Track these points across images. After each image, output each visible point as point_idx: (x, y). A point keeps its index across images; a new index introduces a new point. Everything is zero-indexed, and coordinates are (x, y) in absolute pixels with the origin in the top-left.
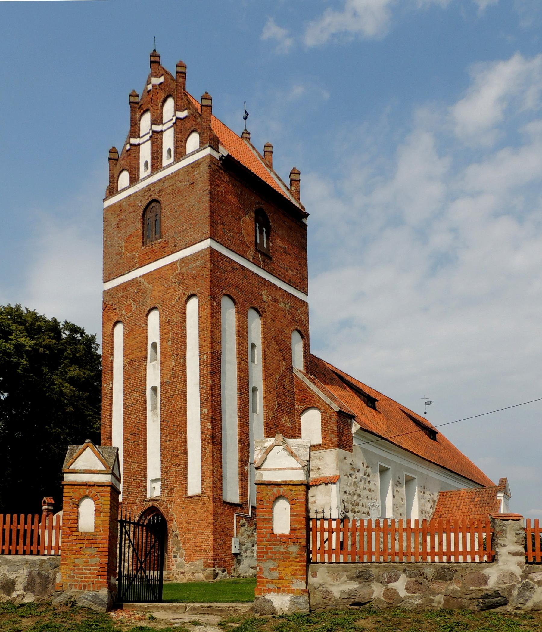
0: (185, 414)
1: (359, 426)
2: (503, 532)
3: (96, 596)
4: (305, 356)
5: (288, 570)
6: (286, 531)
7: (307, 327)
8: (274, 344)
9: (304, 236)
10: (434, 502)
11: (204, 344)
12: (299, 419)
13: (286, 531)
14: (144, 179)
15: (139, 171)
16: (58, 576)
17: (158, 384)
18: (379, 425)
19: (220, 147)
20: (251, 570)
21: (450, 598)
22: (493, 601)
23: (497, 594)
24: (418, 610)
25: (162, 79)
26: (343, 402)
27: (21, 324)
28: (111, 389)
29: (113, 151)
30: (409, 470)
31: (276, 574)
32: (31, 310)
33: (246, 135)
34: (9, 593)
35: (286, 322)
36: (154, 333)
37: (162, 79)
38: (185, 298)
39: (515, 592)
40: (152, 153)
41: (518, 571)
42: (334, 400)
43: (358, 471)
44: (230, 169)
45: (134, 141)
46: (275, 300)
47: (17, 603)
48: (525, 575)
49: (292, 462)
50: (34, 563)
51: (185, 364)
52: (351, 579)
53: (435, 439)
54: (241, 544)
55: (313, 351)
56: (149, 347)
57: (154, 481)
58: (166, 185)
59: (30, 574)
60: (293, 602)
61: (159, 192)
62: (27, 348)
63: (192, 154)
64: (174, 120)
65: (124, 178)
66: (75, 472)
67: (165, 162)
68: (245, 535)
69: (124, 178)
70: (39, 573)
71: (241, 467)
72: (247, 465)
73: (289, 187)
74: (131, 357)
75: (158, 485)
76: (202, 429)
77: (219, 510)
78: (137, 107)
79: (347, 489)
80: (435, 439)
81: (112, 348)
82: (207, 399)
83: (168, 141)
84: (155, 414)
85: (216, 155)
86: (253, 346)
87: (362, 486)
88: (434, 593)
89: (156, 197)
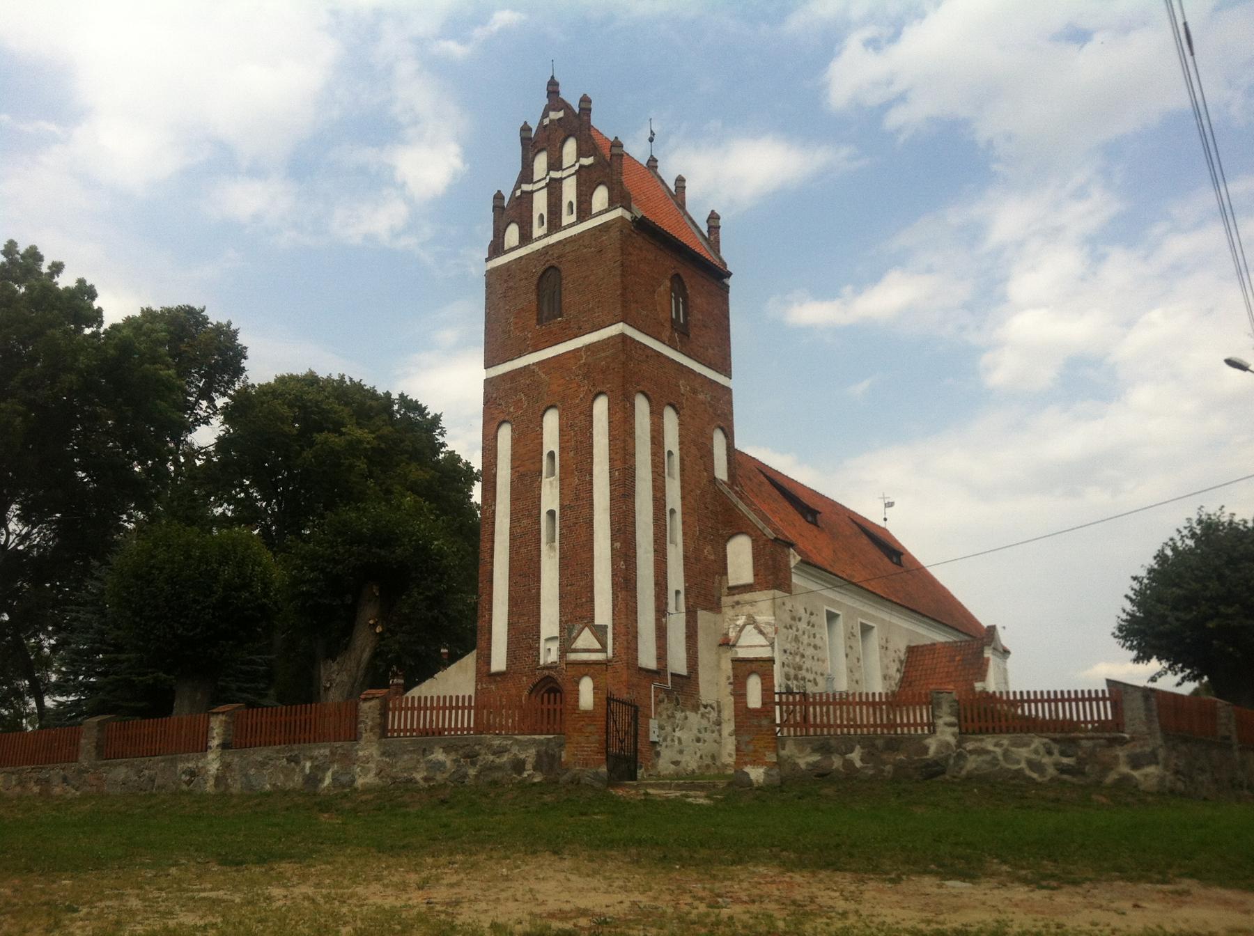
0: (592, 550)
1: (799, 558)
3: (597, 774)
4: (729, 455)
7: (731, 421)
8: (693, 450)
10: (901, 662)
11: (615, 457)
12: (725, 549)
14: (540, 238)
15: (531, 227)
16: (564, 754)
17: (556, 507)
19: (633, 206)
20: (672, 766)
21: (898, 767)
22: (933, 770)
23: (936, 763)
25: (561, 114)
26: (779, 524)
27: (346, 404)
28: (494, 512)
29: (499, 197)
30: (864, 615)
31: (751, 747)
32: (356, 380)
34: (520, 773)
37: (561, 114)
38: (591, 397)
39: (951, 761)
40: (549, 206)
41: (952, 740)
43: (800, 619)
44: (644, 227)
45: (526, 187)
46: (694, 391)
48: (959, 745)
49: (761, 640)
50: (541, 743)
51: (591, 483)
52: (814, 751)
54: (661, 728)
55: (739, 445)
56: (545, 457)
57: (548, 640)
59: (539, 755)
60: (766, 773)
61: (559, 257)
62: (365, 445)
63: (600, 213)
64: (577, 167)
66: (576, 651)
67: (567, 219)
68: (664, 716)
70: (546, 752)
71: (658, 620)
72: (665, 616)
73: (706, 234)
74: (521, 469)
75: (555, 646)
78: (531, 144)
79: (788, 646)
80: (899, 564)
82: (619, 530)
83: (569, 192)
84: (552, 548)
85: (628, 216)
86: (670, 453)
87: (805, 642)
88: (885, 764)
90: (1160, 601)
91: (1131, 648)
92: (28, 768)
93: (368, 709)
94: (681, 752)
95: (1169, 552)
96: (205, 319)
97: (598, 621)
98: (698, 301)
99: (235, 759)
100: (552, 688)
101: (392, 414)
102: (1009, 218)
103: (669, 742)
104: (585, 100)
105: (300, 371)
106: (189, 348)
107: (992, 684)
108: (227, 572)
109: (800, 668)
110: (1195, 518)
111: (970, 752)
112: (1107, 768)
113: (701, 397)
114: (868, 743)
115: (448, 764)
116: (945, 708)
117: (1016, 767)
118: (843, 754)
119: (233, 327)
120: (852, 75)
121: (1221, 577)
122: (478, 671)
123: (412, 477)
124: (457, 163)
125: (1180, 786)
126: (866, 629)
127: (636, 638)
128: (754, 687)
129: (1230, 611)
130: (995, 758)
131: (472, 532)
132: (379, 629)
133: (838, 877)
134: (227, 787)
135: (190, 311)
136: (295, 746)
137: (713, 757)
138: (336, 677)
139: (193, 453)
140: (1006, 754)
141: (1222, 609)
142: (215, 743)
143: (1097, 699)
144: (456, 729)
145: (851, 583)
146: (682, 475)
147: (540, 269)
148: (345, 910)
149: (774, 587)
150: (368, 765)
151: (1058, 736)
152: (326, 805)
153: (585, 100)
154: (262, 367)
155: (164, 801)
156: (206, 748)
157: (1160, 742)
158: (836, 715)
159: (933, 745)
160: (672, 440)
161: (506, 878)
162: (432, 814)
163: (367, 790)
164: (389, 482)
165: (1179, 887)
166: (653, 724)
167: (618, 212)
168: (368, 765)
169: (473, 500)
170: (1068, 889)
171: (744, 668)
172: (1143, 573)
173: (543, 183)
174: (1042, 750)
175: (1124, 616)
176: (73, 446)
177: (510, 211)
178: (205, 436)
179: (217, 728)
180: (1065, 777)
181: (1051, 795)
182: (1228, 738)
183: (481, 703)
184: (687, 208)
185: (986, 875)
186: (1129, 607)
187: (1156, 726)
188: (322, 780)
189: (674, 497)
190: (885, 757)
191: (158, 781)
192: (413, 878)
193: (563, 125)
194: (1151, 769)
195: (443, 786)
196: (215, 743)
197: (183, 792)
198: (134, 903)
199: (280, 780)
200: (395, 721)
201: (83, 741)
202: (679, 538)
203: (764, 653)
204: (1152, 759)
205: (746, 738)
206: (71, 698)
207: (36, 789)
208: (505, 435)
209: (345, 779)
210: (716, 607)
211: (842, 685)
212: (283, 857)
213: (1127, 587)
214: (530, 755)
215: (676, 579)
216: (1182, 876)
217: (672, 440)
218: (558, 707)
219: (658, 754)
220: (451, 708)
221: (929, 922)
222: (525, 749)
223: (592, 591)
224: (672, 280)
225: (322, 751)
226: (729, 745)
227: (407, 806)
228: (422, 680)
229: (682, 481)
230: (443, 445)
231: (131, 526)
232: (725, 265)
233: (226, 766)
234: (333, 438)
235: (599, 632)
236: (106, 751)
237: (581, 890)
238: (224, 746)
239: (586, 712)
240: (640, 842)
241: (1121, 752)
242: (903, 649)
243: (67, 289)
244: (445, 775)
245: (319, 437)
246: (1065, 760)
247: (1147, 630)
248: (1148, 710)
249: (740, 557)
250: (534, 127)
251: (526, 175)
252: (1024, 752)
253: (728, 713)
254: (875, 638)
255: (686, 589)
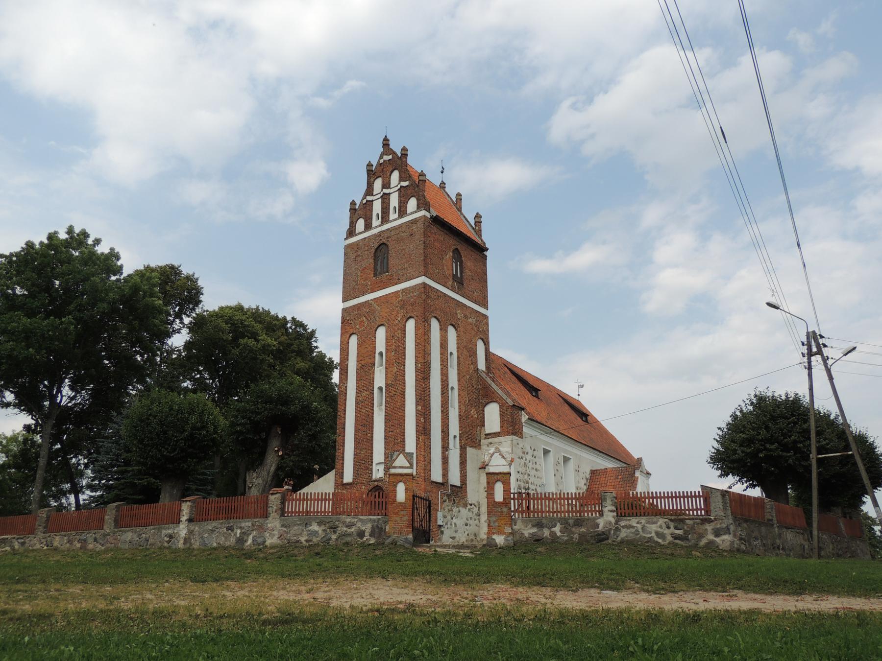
1: (527, 417)
2: (605, 499)
5: (503, 522)
6: (501, 500)
7: (488, 335)
8: (465, 352)
9: (485, 265)
10: (587, 479)
12: (483, 411)
13: (501, 500)
14: (376, 227)
16: (387, 528)
18: (541, 412)
21: (582, 536)
22: (602, 537)
23: (603, 533)
24: (566, 542)
27: (260, 322)
29: (353, 203)
30: (565, 451)
33: (443, 185)
35: (473, 333)
36: (381, 344)
37: (390, 157)
40: (382, 208)
41: (613, 521)
42: (509, 395)
45: (369, 198)
46: (466, 317)
47: (367, 543)
48: (616, 523)
49: (503, 462)
50: (374, 521)
51: (404, 371)
52: (533, 526)
53: (586, 421)
54: (445, 517)
55: (492, 350)
56: (377, 355)
58: (393, 233)
61: (388, 238)
63: (412, 213)
65: (360, 224)
66: (395, 467)
67: (393, 216)
69: (360, 224)
71: (443, 453)
72: (447, 450)
75: (382, 468)
76: (417, 423)
77: (429, 489)
78: (372, 174)
79: (520, 470)
80: (586, 421)
81: (348, 355)
83: (394, 201)
85: (428, 215)
86: (451, 353)
89: (385, 241)
90: (733, 441)
91: (717, 469)
92: (74, 533)
93: (274, 500)
94: (456, 531)
95: (738, 413)
96: (181, 271)
97: (407, 451)
98: (469, 264)
99: (196, 528)
100: (378, 496)
101: (287, 329)
102: (652, 214)
103: (449, 526)
104: (404, 149)
105: (233, 303)
106: (173, 288)
107: (640, 488)
108: (193, 419)
109: (527, 483)
110: (753, 394)
111: (623, 527)
112: (701, 536)
113: (470, 320)
114: (564, 522)
115: (320, 532)
116: (609, 502)
117: (649, 536)
118: (550, 528)
119: (196, 276)
120: (564, 124)
121: (767, 428)
122: (336, 481)
123: (297, 366)
124: (324, 172)
125: (743, 547)
126: (566, 460)
127: (430, 463)
128: (499, 488)
129: (773, 447)
130: (637, 531)
131: (333, 400)
132: (280, 453)
133: (544, 589)
134: (191, 544)
135: (172, 267)
136: (231, 521)
137: (475, 535)
138: (256, 481)
139: (172, 351)
140: (643, 528)
141: (768, 446)
142: (184, 518)
143: (695, 497)
144: (325, 512)
145: (558, 432)
146: (458, 367)
147: (376, 245)
148: (267, 600)
149: (512, 434)
150: (274, 531)
151: (673, 518)
152: (248, 555)
153: (404, 149)
154: (212, 301)
155: (154, 553)
156: (179, 522)
157: (731, 521)
158: (545, 505)
159: (601, 522)
160: (452, 346)
161: (356, 589)
162: (311, 560)
163: (273, 547)
164: (284, 369)
165: (731, 594)
166: (440, 515)
167: (423, 213)
168: (274, 531)
169: (333, 381)
170: (671, 594)
171: (493, 478)
172: (724, 426)
173: (379, 196)
174: (664, 526)
175: (713, 450)
176: (101, 345)
177: (360, 211)
178: (178, 340)
179: (186, 509)
180: (677, 541)
181: (669, 552)
182: (771, 520)
183: (336, 499)
184: (463, 211)
185: (626, 589)
186: (716, 445)
187: (729, 512)
188: (246, 541)
189: (453, 380)
190: (574, 529)
191: (151, 541)
192: (303, 588)
193: (392, 162)
194: (726, 537)
195: (317, 545)
196: (184, 518)
197: (165, 547)
198: (149, 596)
199: (222, 540)
200: (289, 507)
201: (107, 517)
202: (456, 405)
203: (505, 469)
204: (727, 531)
205: (494, 519)
206: (98, 493)
207: (78, 545)
208: (354, 341)
209: (260, 540)
210: (477, 445)
211: (552, 489)
212: (227, 579)
213: (715, 434)
214: (367, 528)
215: (454, 429)
216: (734, 588)
217: (452, 346)
218: (384, 500)
219: (442, 532)
220: (318, 500)
221: (590, 607)
222: (365, 524)
223: (404, 435)
224: (453, 252)
225: (247, 524)
226: (484, 529)
227: (296, 556)
228: (307, 484)
229: (458, 370)
230: (317, 347)
231: (133, 392)
232: (484, 243)
233: (191, 532)
234: (251, 342)
235: (408, 456)
236: (119, 523)
237: (399, 594)
238: (190, 520)
239: (400, 503)
240: (431, 573)
241: (709, 527)
242: (588, 472)
243: (102, 254)
244: (319, 539)
245: (243, 341)
246: (677, 532)
247: (727, 459)
248: (724, 502)
249: (492, 415)
250: (375, 164)
251: (369, 191)
252: (654, 528)
253: (484, 509)
254: (571, 465)
255: (460, 435)
